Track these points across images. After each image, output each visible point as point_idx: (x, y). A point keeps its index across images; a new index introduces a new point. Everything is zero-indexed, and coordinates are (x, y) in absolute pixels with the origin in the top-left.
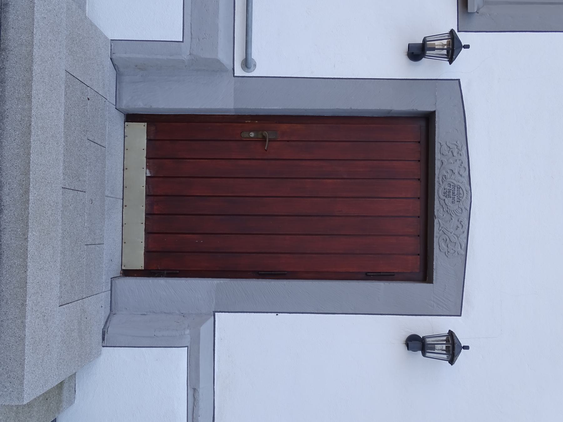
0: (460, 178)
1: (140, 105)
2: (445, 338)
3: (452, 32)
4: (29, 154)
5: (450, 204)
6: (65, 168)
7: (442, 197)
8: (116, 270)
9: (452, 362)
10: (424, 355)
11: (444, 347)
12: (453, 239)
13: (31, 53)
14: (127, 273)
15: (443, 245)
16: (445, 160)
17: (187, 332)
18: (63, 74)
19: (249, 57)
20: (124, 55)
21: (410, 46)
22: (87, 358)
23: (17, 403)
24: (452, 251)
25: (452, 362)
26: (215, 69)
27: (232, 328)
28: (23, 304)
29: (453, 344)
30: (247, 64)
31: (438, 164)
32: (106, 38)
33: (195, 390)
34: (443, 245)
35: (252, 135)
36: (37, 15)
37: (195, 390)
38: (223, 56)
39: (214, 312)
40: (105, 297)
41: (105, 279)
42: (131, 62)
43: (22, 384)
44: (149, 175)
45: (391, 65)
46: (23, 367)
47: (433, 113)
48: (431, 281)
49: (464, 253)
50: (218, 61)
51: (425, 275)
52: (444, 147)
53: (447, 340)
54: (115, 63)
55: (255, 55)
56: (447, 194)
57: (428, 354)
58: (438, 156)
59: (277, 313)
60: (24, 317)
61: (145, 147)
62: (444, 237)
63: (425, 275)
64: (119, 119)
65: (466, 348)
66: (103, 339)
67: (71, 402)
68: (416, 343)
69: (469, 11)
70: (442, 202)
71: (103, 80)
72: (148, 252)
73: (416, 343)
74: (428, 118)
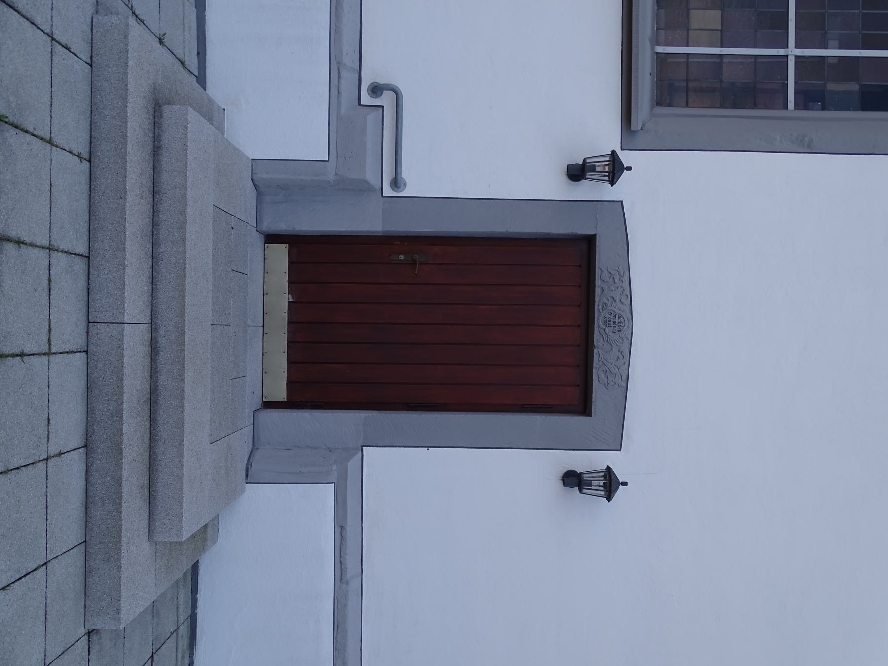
0: (621, 306)
1: (282, 227)
2: (603, 474)
3: (613, 152)
4: (184, 296)
5: (610, 334)
6: (213, 305)
7: (602, 326)
8: (257, 403)
9: (609, 498)
10: (580, 492)
11: (602, 483)
12: (613, 370)
13: (184, 196)
14: (269, 405)
15: (603, 376)
16: (605, 286)
17: (334, 467)
18: (212, 208)
19: (399, 178)
20: (265, 176)
21: (570, 167)
22: (231, 496)
23: (175, 539)
24: (612, 383)
25: (609, 498)
26: (362, 189)
27: (375, 459)
28: (180, 444)
29: (610, 480)
30: (396, 183)
31: (598, 291)
32: (248, 158)
33: (342, 528)
34: (603, 376)
35: (402, 257)
36: (190, 158)
37: (342, 527)
38: (371, 176)
39: (362, 447)
40: (247, 431)
41: (248, 413)
42: (272, 183)
43: (180, 521)
44: (291, 300)
45: (551, 186)
46: (182, 505)
47: (595, 236)
48: (590, 415)
49: (624, 385)
50: (366, 181)
51: (584, 408)
52: (606, 273)
53: (604, 476)
54: (256, 182)
55: (405, 174)
56: (607, 323)
57: (584, 491)
58: (598, 282)
59: (428, 447)
60: (182, 456)
61: (287, 271)
62: (604, 367)
63: (584, 408)
64: (259, 240)
65: (625, 484)
66: (247, 475)
67: (214, 541)
68: (573, 480)
69: (633, 129)
70: (602, 331)
71: (244, 204)
72: (290, 383)
73: (573, 480)
74: (590, 241)
